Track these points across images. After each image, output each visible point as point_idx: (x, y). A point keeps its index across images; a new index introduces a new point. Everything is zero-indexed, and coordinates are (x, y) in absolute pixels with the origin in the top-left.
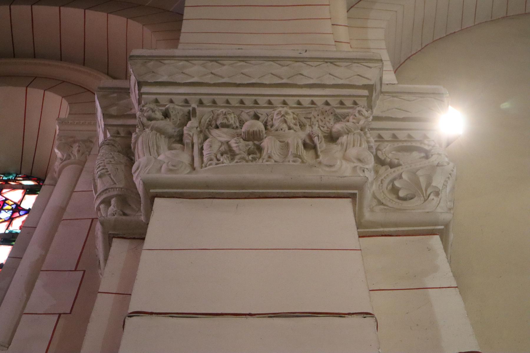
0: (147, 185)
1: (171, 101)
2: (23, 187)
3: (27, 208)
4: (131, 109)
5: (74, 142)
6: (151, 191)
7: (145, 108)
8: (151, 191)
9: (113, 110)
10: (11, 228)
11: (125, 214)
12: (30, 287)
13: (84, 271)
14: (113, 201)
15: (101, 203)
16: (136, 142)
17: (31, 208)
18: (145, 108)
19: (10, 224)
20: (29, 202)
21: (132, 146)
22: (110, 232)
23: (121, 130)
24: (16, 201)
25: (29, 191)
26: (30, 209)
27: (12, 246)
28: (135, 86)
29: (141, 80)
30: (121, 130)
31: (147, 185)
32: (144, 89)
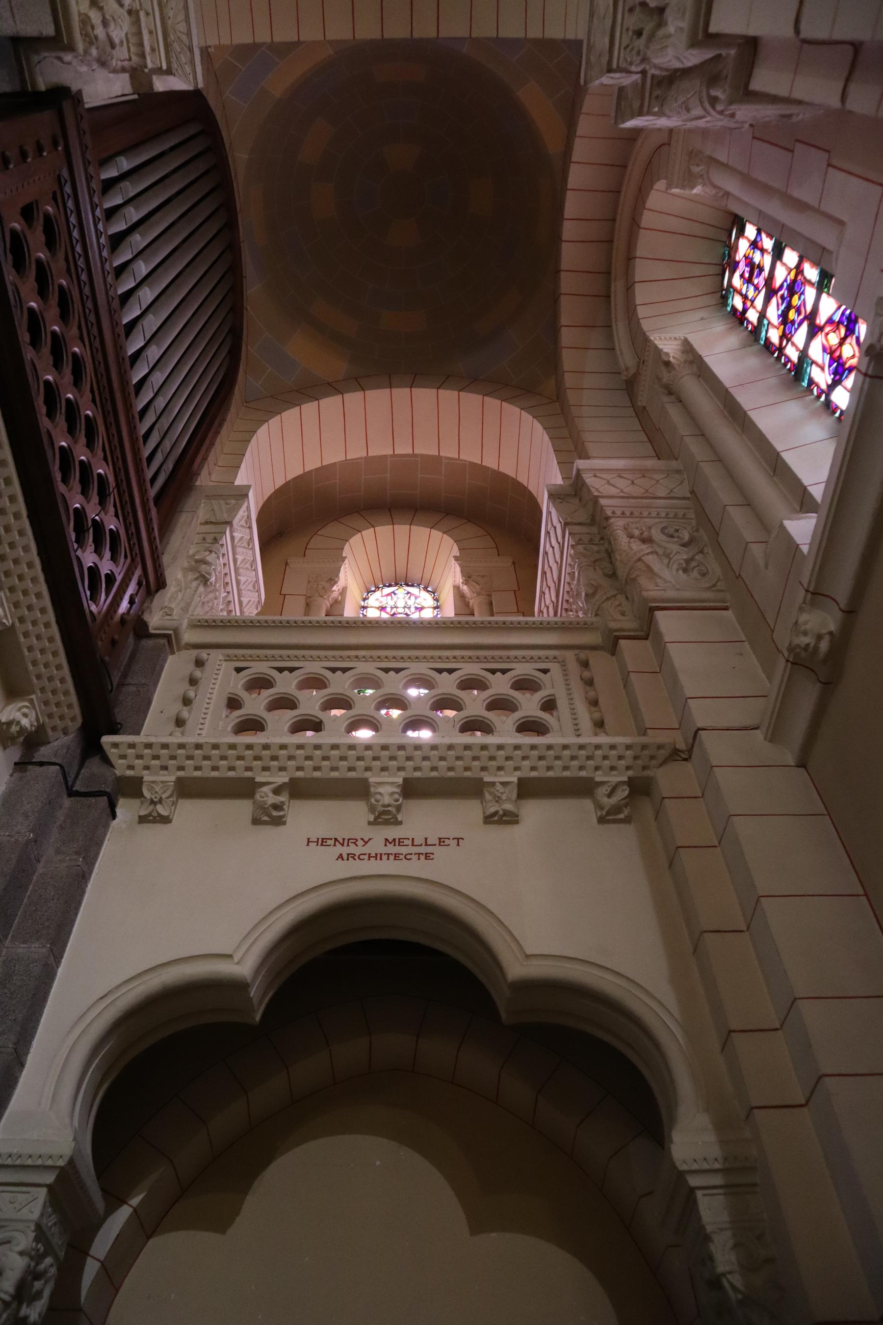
0: (693, 43)
1: (628, 30)
2: (737, 238)
3: (756, 232)
4: (637, 84)
5: (689, 171)
6: (700, 37)
7: (629, 60)
8: (700, 37)
9: (636, 105)
10: (770, 250)
11: (726, 77)
12: (801, 206)
13: (797, 140)
14: (713, 93)
15: (713, 107)
16: (661, 69)
17: (756, 228)
18: (629, 60)
19: (766, 250)
20: (751, 231)
21: (665, 73)
22: (741, 93)
23: (655, 94)
24: (748, 244)
25: (741, 232)
26: (757, 229)
27: (804, 259)
28: (612, 78)
29: (605, 70)
30: (655, 94)
31: (693, 43)
32: (615, 66)
